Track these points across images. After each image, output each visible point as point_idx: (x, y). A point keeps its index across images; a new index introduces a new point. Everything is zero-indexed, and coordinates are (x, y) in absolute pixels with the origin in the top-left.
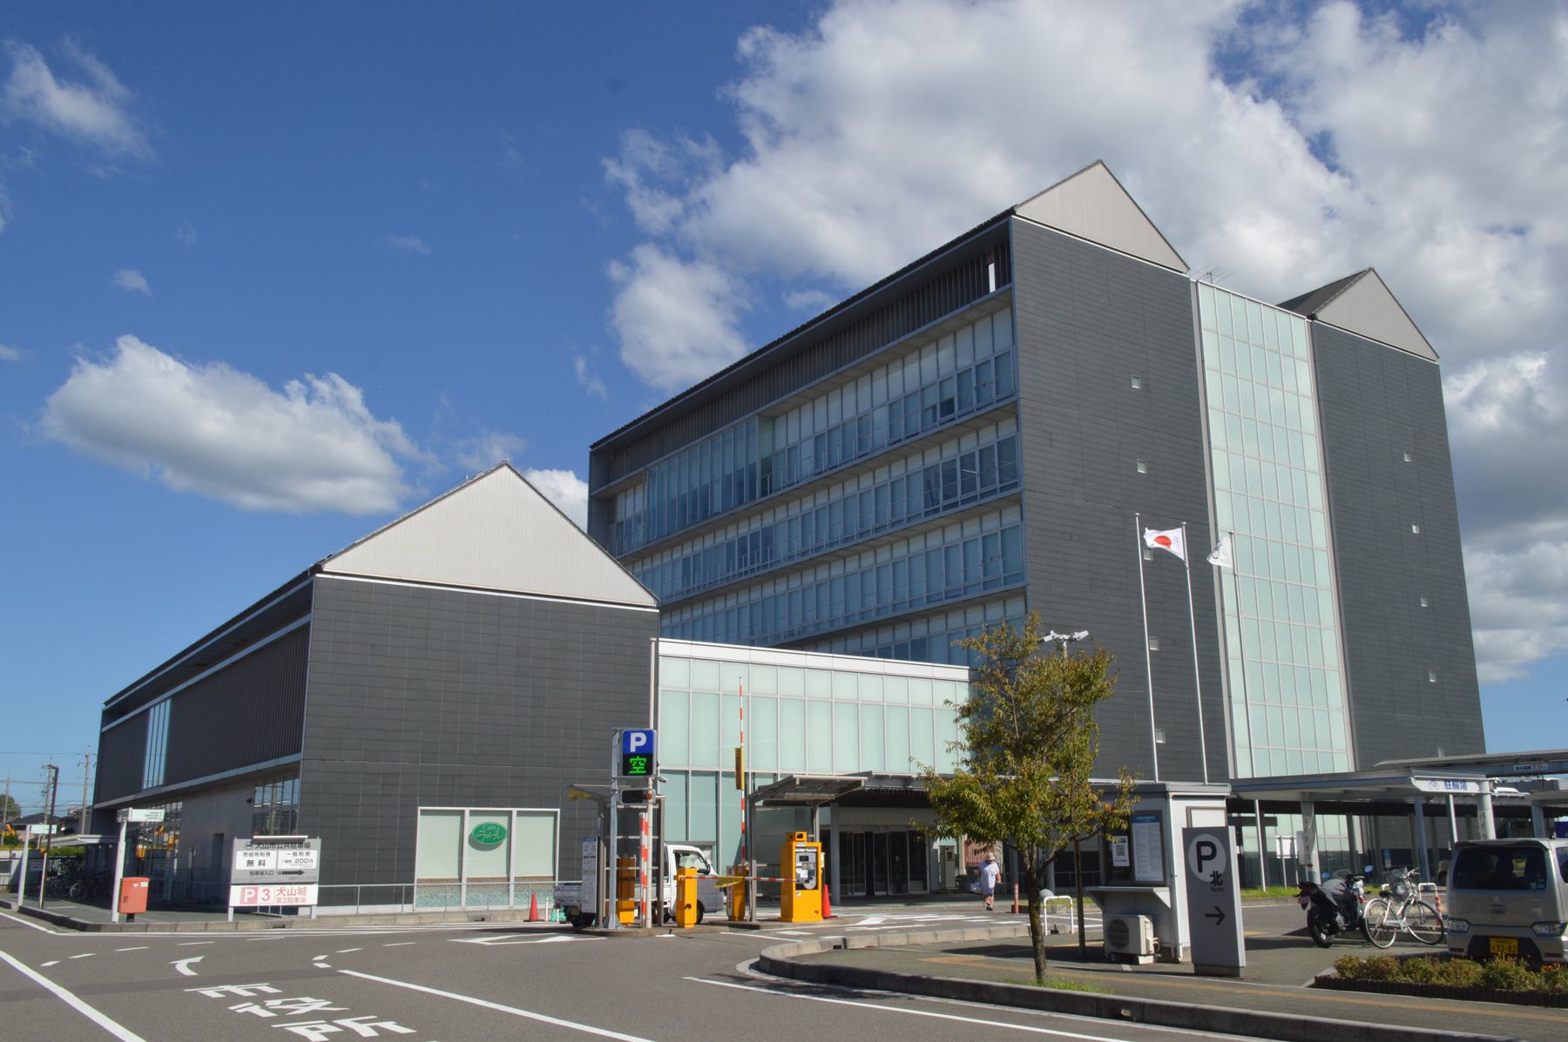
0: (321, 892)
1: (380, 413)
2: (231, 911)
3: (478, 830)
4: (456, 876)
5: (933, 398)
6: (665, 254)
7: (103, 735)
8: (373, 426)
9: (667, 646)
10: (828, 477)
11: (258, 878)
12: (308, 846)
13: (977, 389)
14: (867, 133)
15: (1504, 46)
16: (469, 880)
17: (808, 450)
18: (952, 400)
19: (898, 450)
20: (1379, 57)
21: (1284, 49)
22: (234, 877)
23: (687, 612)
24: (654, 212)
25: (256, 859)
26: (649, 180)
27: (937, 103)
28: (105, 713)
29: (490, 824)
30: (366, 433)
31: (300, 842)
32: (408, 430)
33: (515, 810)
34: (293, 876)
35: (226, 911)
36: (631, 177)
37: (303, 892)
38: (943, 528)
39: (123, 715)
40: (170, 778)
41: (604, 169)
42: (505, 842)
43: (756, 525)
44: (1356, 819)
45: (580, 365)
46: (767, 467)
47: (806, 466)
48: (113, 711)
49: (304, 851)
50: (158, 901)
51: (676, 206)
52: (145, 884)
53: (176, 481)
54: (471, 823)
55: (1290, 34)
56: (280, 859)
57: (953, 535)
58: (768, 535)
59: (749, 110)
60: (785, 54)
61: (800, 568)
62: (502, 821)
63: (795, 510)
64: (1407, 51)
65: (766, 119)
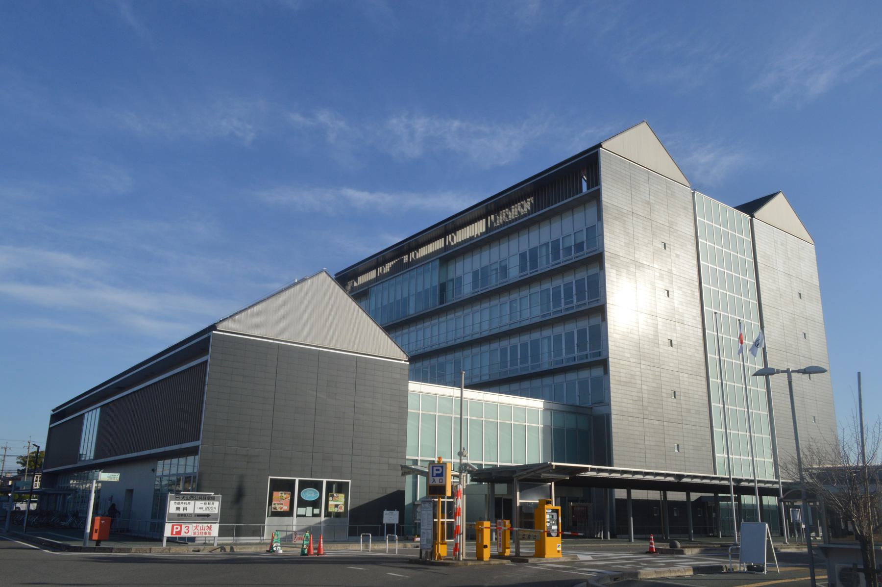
2: (165, 540)
7: (50, 429)
11: (184, 517)
23: (428, 363)
25: (181, 506)
28: (52, 416)
35: (161, 541)
37: (210, 528)
39: (65, 419)
40: (98, 453)
48: (58, 415)
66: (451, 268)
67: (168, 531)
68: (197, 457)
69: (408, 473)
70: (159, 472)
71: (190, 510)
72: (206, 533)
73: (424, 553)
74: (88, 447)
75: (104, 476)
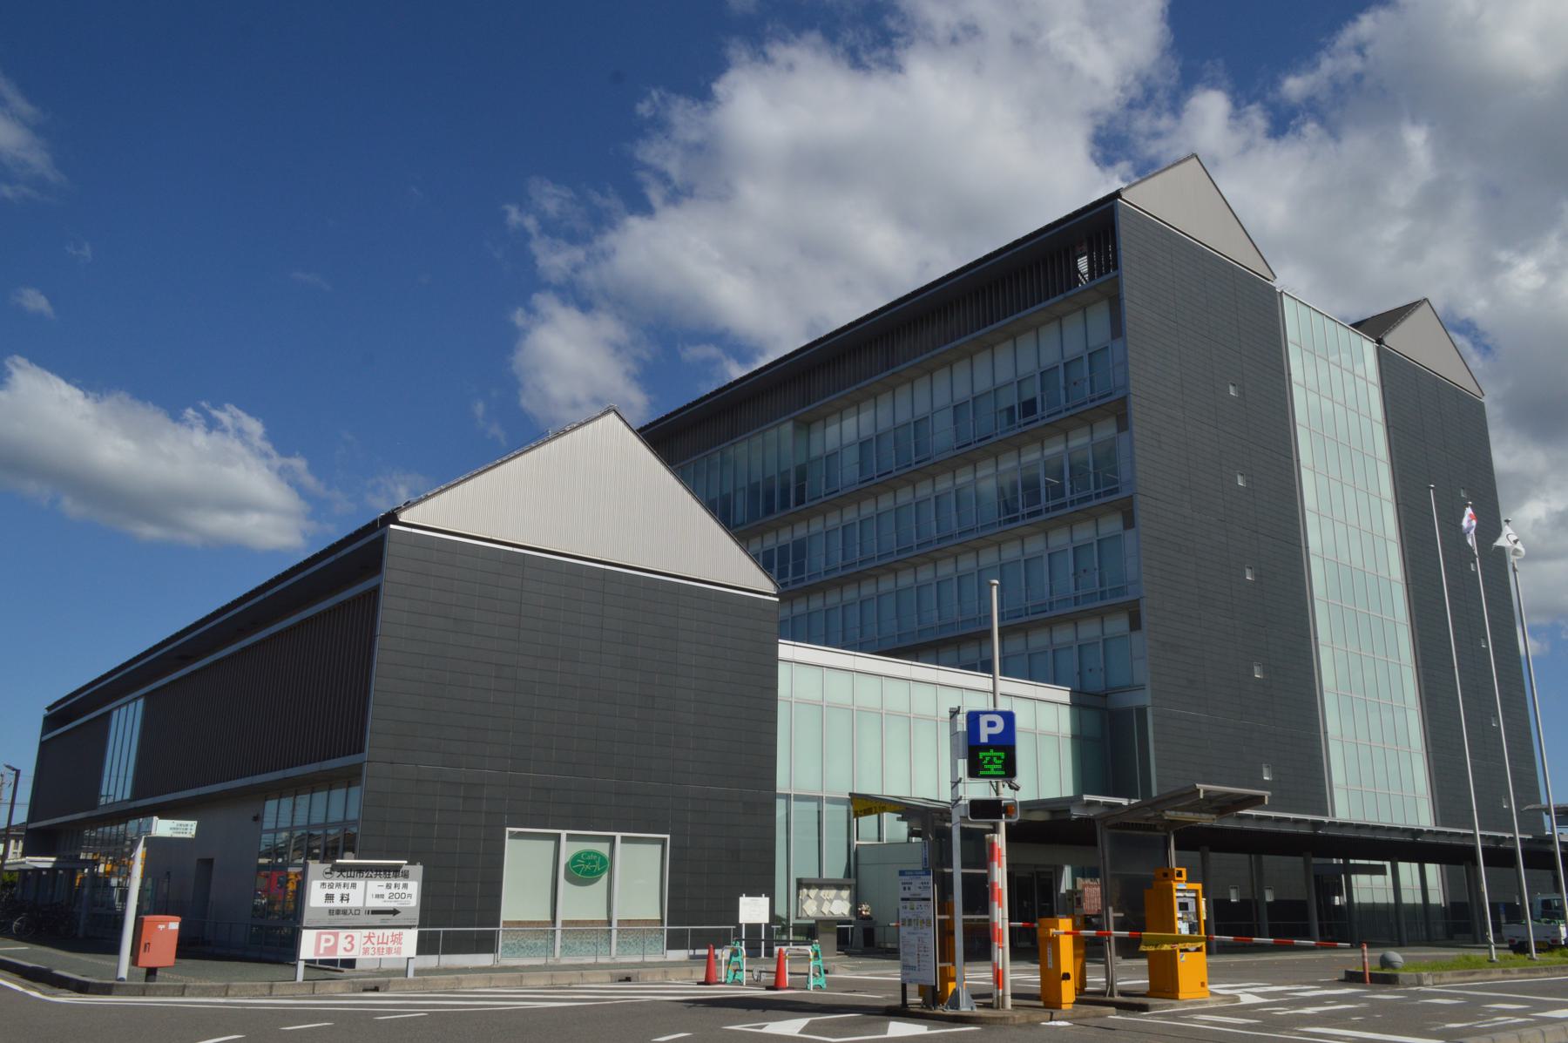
0: (421, 937)
1: (285, 449)
2: (301, 965)
3: (575, 859)
4: (605, 918)
5: (1010, 399)
6: (565, 303)
7: (43, 745)
8: (278, 461)
9: (786, 650)
10: (873, 485)
11: (341, 919)
12: (406, 876)
13: (1066, 389)
14: (759, 197)
15: (1357, 144)
16: (565, 923)
17: (851, 457)
18: (1033, 401)
19: (968, 454)
20: (1248, 146)
21: (1156, 135)
22: (307, 918)
24: (555, 260)
25: (337, 892)
26: (549, 228)
27: (823, 167)
28: (47, 719)
29: (589, 853)
30: (269, 467)
31: (396, 870)
32: (313, 468)
33: (618, 835)
34: (386, 917)
36: (530, 223)
38: (1022, 538)
39: (73, 728)
40: (139, 791)
41: (506, 213)
42: (605, 876)
43: (785, 537)
44: (1432, 870)
45: (479, 408)
46: (802, 473)
47: (849, 470)
48: (57, 717)
49: (401, 882)
50: (190, 947)
51: (579, 254)
52: (174, 925)
53: (71, 507)
54: (568, 850)
55: (1165, 122)
56: (368, 892)
57: (1035, 546)
58: (800, 548)
59: (646, 167)
60: (681, 113)
61: (840, 583)
62: (603, 848)
63: (833, 520)
64: (1271, 145)
65: (664, 178)
66: (816, 437)
67: (311, 945)
68: (355, 792)
69: (868, 812)
70: (268, 823)
71: (356, 901)
72: (389, 950)
73: (912, 989)
74: (117, 783)
75: (163, 828)
